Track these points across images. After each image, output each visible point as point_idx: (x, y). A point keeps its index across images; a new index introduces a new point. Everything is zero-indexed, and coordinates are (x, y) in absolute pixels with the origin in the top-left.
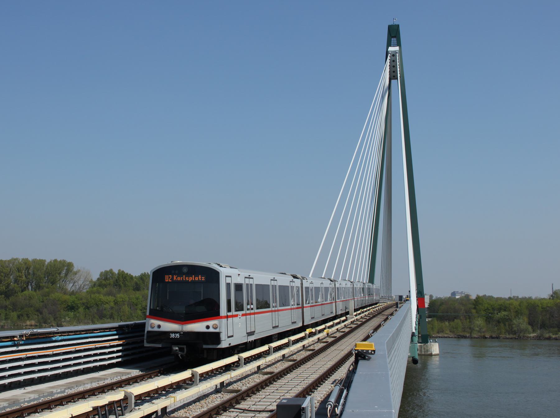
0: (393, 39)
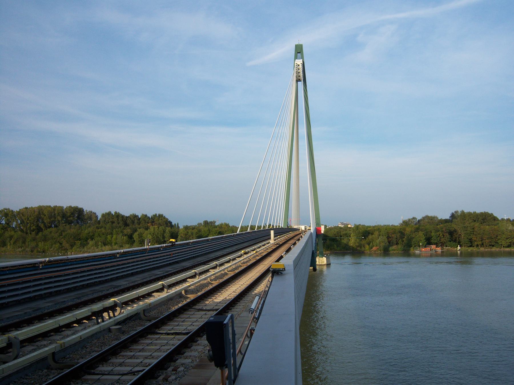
0: (298, 54)
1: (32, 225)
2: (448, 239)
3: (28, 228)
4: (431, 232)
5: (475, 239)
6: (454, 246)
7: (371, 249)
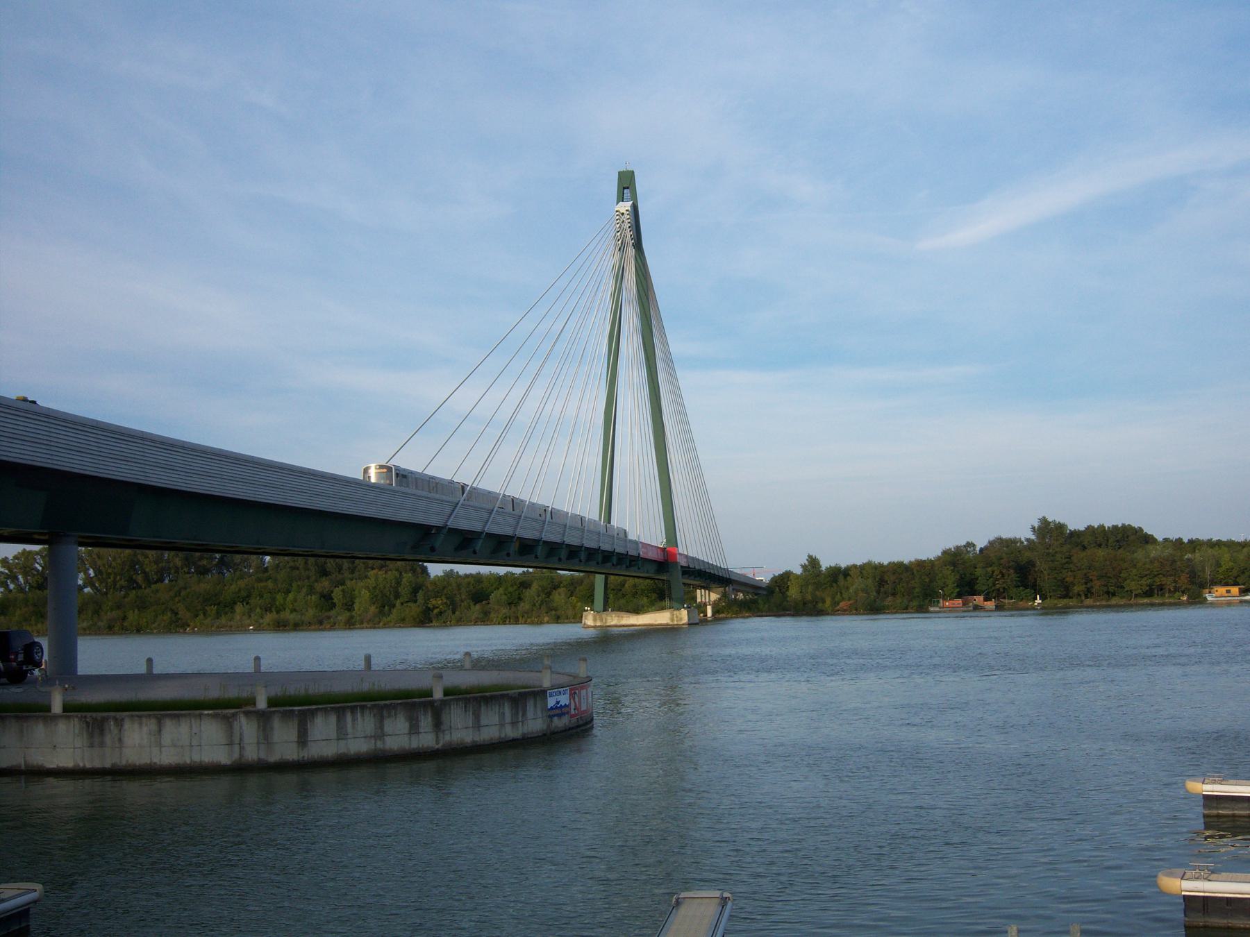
1: (118, 577)
2: (1012, 581)
3: (109, 584)
4: (976, 568)
5: (1072, 579)
6: (1026, 596)
7: (836, 607)
